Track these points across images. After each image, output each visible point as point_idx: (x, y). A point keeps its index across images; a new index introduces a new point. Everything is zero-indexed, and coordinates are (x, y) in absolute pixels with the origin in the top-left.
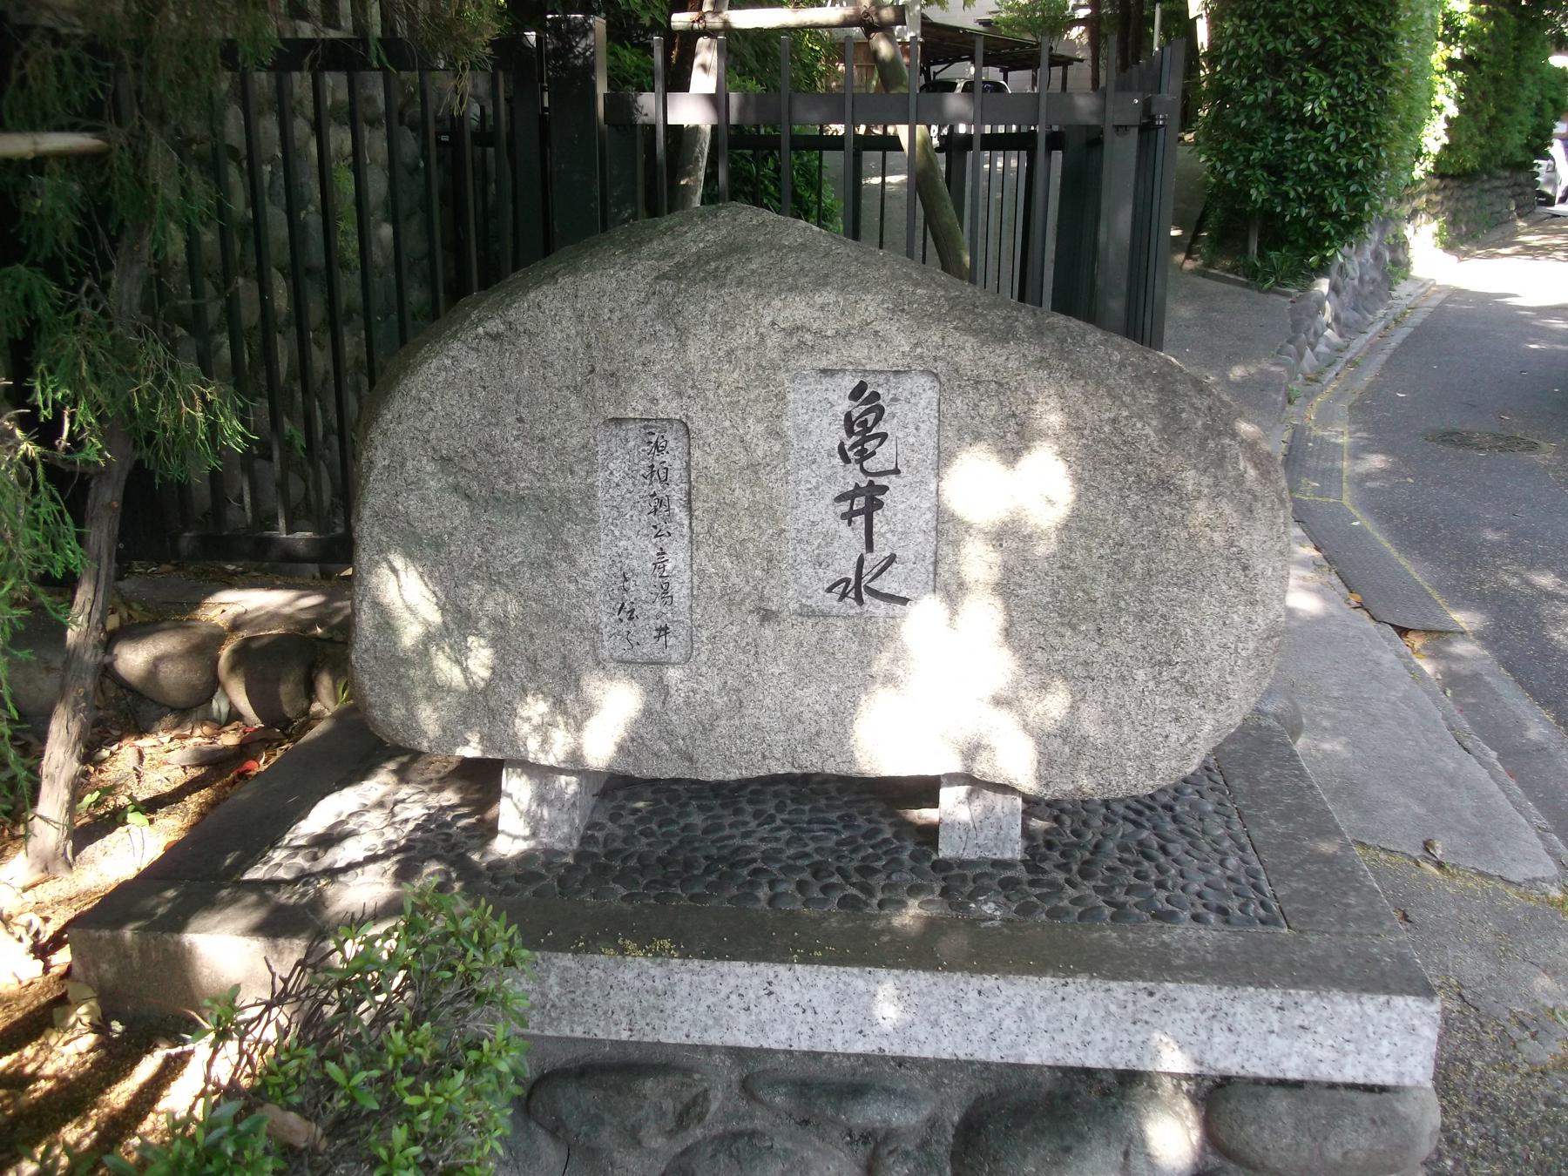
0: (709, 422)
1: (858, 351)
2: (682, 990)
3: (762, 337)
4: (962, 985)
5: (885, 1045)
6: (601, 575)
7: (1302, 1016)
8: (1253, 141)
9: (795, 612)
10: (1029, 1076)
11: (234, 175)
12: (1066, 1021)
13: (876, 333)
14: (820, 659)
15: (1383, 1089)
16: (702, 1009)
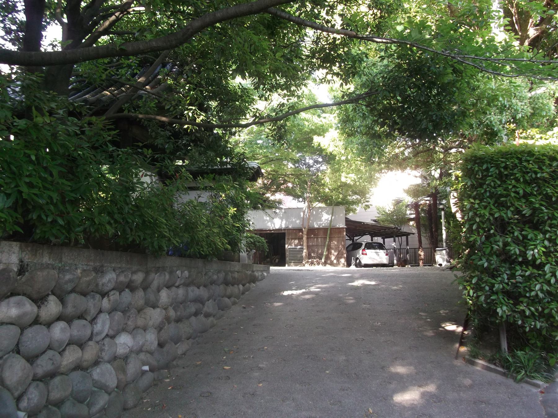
8: (494, 277)
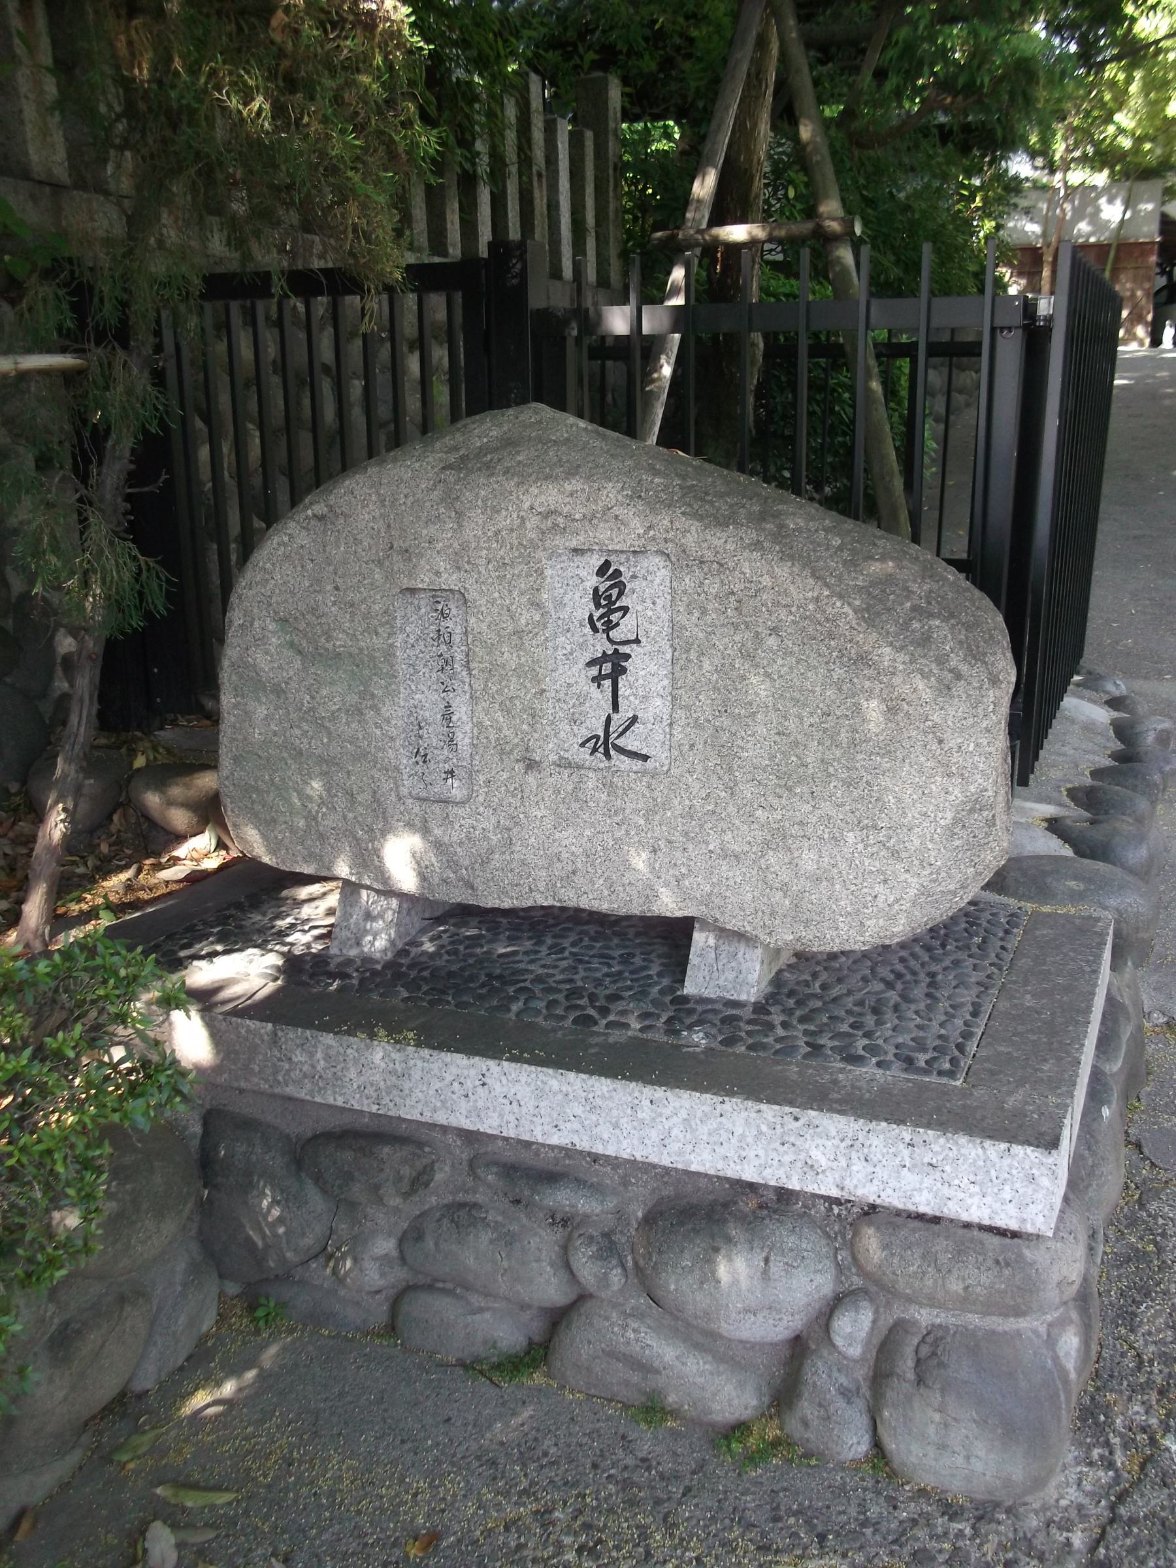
0: (481, 593)
1: (603, 533)
2: (416, 1075)
3: (523, 520)
4: (636, 1094)
5: (576, 1140)
6: (400, 723)
7: (930, 1155)
9: (554, 763)
10: (703, 1183)
11: (326, 387)
12: (724, 1136)
13: (617, 517)
14: (575, 806)
15: (1015, 1235)
16: (432, 1092)
